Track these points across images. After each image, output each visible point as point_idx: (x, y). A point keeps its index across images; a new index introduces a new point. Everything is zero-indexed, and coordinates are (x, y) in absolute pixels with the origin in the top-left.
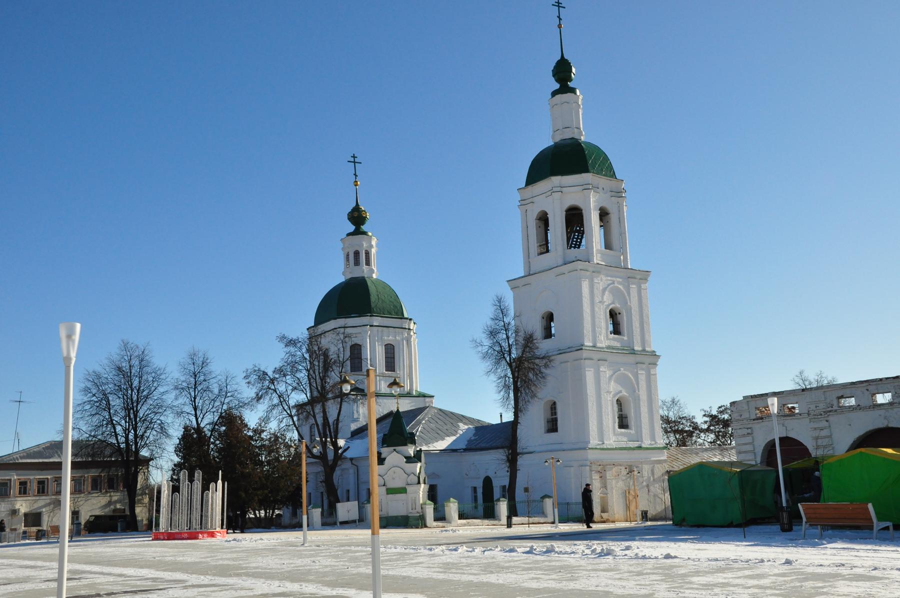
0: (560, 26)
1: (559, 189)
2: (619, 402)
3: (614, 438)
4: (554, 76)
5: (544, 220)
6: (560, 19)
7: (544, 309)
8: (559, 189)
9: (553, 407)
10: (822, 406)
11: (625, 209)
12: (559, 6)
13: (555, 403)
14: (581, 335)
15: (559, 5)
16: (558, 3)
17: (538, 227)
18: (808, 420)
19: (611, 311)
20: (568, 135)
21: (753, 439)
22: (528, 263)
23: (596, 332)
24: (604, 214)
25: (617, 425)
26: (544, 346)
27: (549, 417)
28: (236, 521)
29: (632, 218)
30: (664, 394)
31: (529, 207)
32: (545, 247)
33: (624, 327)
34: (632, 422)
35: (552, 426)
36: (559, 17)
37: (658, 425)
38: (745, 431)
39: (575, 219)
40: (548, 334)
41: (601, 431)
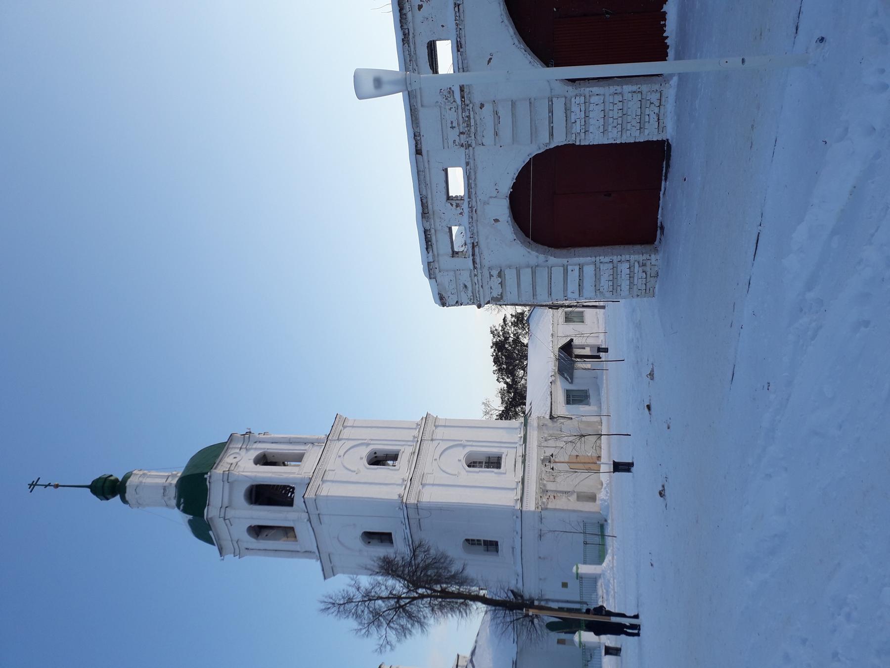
0: (57, 486)
1: (223, 510)
2: (472, 464)
3: (509, 475)
4: (108, 499)
5: (257, 531)
6: (49, 485)
7: (359, 544)
8: (223, 510)
9: (471, 543)
10: (451, 116)
11: (276, 436)
12: (36, 484)
13: (467, 540)
14: (387, 503)
15: (33, 485)
16: (31, 485)
17: (267, 538)
18: (479, 150)
19: (469, 466)
20: (172, 492)
21: (510, 267)
22: (307, 553)
23: (386, 485)
24: (264, 460)
25: (495, 470)
26: (400, 549)
27: (482, 547)
28: (665, 20)
29: (278, 430)
30: (477, 414)
31: (244, 545)
32: (288, 531)
33: (390, 448)
34: (494, 450)
35: (491, 546)
36: (46, 486)
37: (505, 423)
38: (496, 281)
39: (264, 495)
40: (385, 538)
41: (493, 491)
